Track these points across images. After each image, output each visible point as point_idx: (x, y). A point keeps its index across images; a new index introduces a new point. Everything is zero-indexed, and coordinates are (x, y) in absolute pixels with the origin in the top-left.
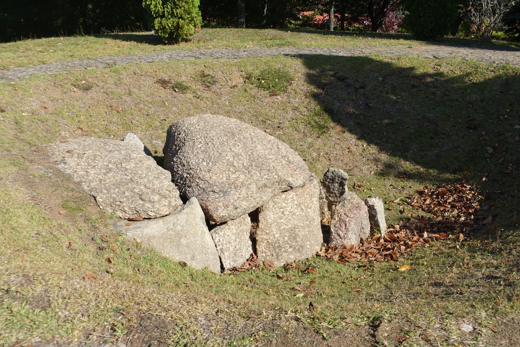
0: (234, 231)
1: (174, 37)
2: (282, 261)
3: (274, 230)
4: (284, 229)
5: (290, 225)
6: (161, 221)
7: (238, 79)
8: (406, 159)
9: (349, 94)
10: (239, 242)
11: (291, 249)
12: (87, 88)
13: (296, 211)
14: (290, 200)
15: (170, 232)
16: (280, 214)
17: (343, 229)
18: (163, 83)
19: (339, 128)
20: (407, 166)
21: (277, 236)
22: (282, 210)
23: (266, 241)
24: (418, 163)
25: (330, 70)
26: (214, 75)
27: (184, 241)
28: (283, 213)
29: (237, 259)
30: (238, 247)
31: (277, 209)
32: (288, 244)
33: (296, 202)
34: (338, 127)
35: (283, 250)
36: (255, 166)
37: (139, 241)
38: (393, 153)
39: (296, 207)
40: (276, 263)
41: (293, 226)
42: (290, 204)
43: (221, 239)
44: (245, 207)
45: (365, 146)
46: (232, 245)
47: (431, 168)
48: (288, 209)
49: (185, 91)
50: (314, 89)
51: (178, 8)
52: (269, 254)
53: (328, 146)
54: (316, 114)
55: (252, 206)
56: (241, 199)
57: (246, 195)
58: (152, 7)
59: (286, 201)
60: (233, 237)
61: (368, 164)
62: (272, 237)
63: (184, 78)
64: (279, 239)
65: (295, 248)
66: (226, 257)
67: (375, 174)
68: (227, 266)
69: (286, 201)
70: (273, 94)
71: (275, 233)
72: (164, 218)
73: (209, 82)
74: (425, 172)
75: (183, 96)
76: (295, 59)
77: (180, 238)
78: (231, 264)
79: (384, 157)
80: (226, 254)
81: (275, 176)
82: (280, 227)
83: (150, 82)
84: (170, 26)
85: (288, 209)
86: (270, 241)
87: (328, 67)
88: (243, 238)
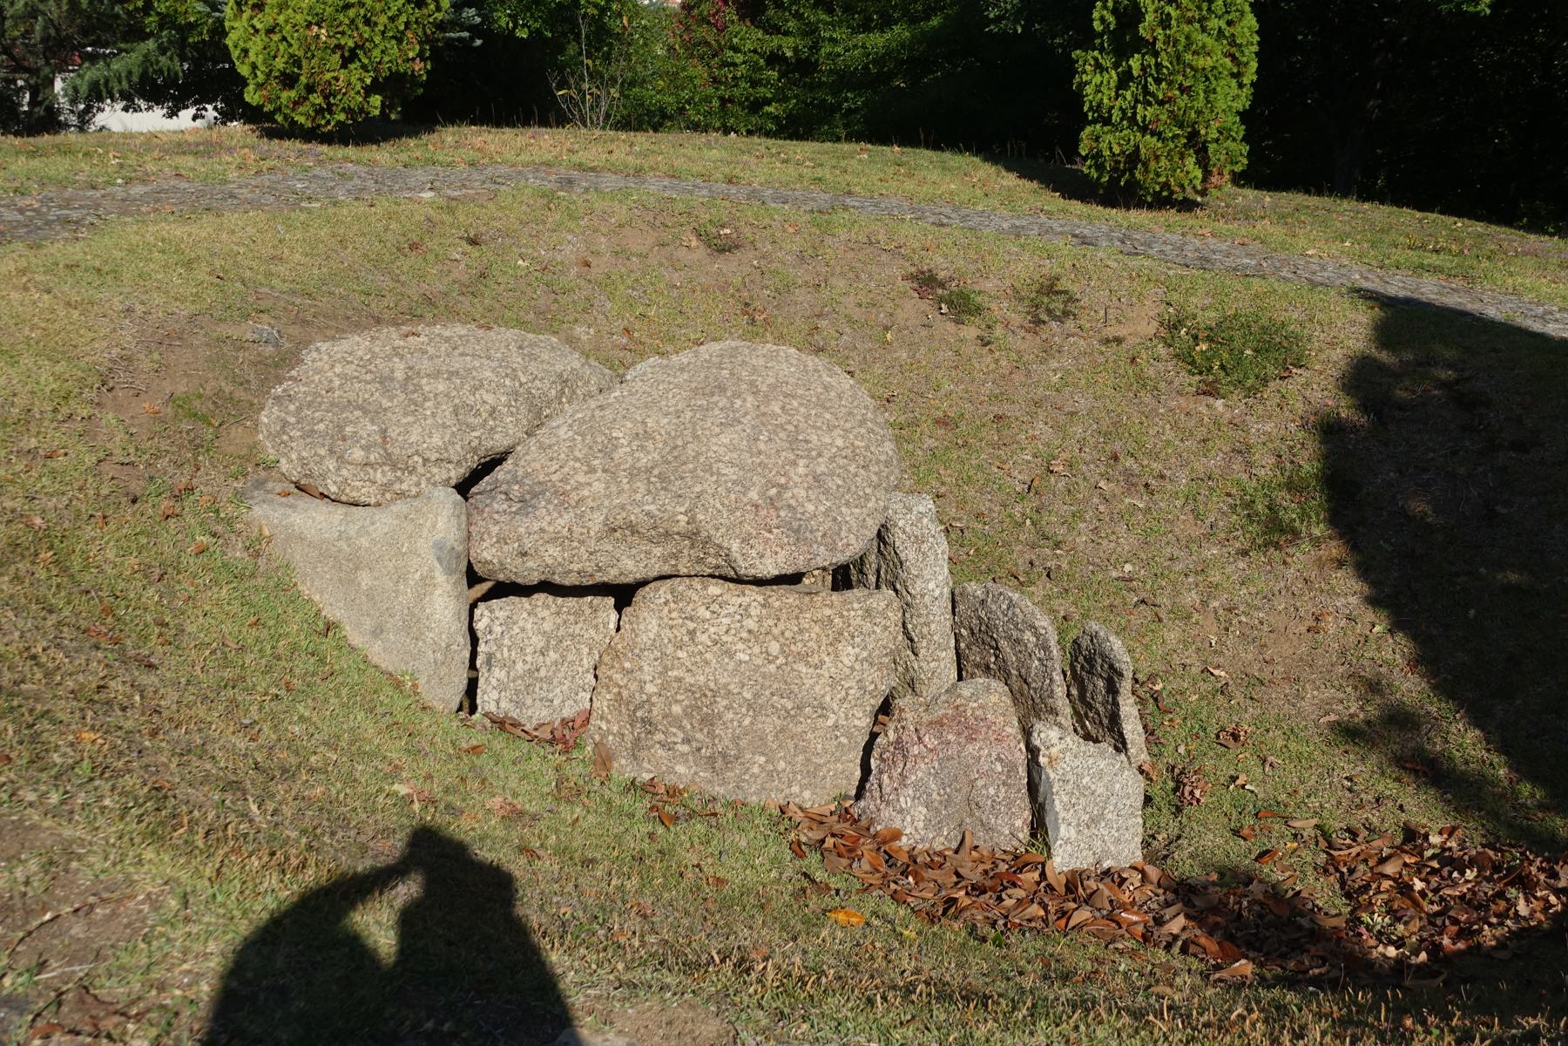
0: (547, 626)
1: (1120, 189)
2: (645, 765)
3: (646, 668)
4: (679, 680)
5: (702, 678)
6: (341, 510)
7: (1144, 323)
8: (1478, 718)
9: (1455, 453)
10: (556, 663)
11: (685, 748)
12: (723, 248)
13: (740, 646)
14: (732, 610)
15: (343, 544)
16: (681, 633)
17: (895, 775)
18: (926, 282)
19: (1334, 549)
20: (1464, 742)
21: (651, 688)
22: (691, 625)
23: (616, 690)
24: (1504, 748)
25: (1450, 366)
26: (1078, 296)
27: (365, 579)
28: (692, 633)
29: (529, 702)
30: (543, 673)
31: (674, 615)
32: (681, 728)
33: (750, 623)
34: (1334, 543)
35: (659, 737)
36: (659, 476)
37: (267, 533)
38: (1447, 683)
39: (744, 635)
40: (623, 762)
41: (712, 685)
42: (726, 621)
43: (498, 629)
44: (550, 561)
45: (1377, 629)
46: (529, 659)
47: (1535, 779)
48: (712, 630)
49: (965, 317)
50: (1345, 409)
51: (1150, 104)
52: (615, 729)
53: (1253, 590)
54: (1290, 486)
55: (575, 567)
56: (546, 537)
57: (565, 532)
58: (1089, 89)
59: (715, 607)
60: (538, 641)
61: (1340, 688)
62: (634, 686)
63: (989, 285)
64: (654, 699)
65: (699, 750)
66: (494, 682)
67: (1332, 726)
68: (488, 699)
69: (715, 607)
70: (1211, 391)
71: (648, 678)
72: (354, 509)
73: (1049, 312)
74: (1506, 783)
75: (951, 327)
76: (1362, 305)
77: (357, 569)
78: (503, 705)
79: (1410, 688)
80: (498, 673)
81: (680, 517)
82: (666, 669)
83: (897, 270)
84: (1117, 150)
85: (712, 630)
86: (625, 693)
87: (1449, 354)
88: (570, 657)
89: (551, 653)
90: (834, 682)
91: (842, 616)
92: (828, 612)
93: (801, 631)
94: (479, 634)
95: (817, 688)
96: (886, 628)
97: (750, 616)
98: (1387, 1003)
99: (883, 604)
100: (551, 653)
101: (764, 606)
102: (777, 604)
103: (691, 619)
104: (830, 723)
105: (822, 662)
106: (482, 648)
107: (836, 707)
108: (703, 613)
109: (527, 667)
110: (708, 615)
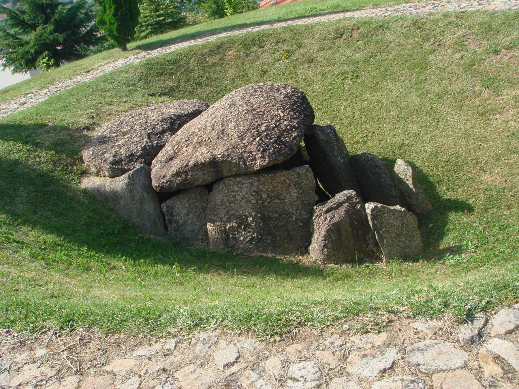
0: (187, 205)
4: (233, 214)
5: (241, 212)
13: (252, 198)
14: (246, 185)
22: (233, 194)
28: (234, 196)
42: (245, 190)
46: (183, 218)
48: (241, 194)
85: (241, 194)
89: (191, 215)
90: (291, 204)
91: (289, 179)
92: (282, 178)
93: (274, 187)
94: (165, 213)
95: (286, 207)
96: (308, 179)
97: (253, 186)
98: (164, 20)
99: (304, 171)
100: (191, 215)
101: (257, 181)
102: (263, 180)
103: (233, 192)
104: (294, 219)
105: (285, 197)
106: (167, 218)
107: (295, 213)
108: (236, 188)
109: (183, 221)
110: (238, 189)
